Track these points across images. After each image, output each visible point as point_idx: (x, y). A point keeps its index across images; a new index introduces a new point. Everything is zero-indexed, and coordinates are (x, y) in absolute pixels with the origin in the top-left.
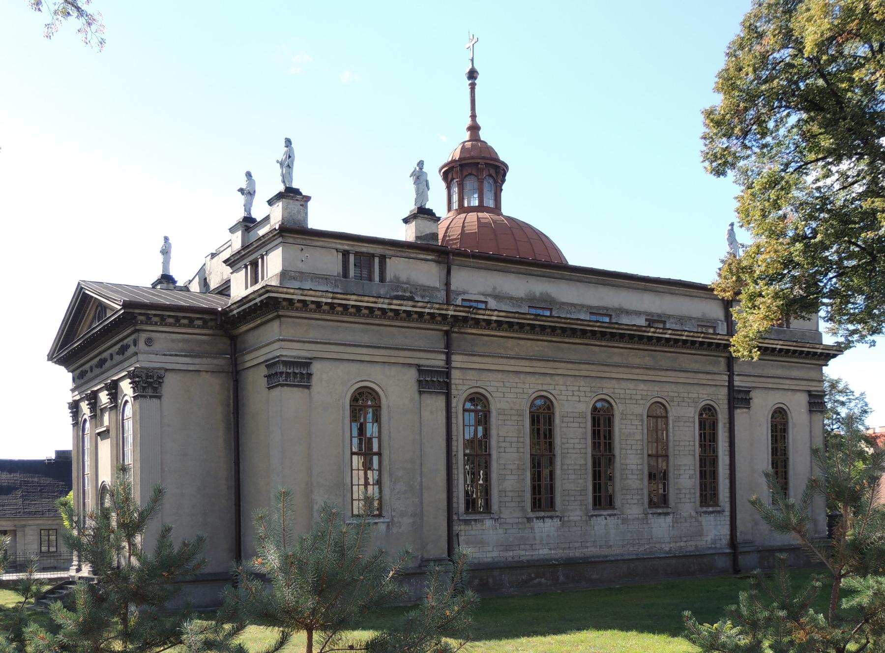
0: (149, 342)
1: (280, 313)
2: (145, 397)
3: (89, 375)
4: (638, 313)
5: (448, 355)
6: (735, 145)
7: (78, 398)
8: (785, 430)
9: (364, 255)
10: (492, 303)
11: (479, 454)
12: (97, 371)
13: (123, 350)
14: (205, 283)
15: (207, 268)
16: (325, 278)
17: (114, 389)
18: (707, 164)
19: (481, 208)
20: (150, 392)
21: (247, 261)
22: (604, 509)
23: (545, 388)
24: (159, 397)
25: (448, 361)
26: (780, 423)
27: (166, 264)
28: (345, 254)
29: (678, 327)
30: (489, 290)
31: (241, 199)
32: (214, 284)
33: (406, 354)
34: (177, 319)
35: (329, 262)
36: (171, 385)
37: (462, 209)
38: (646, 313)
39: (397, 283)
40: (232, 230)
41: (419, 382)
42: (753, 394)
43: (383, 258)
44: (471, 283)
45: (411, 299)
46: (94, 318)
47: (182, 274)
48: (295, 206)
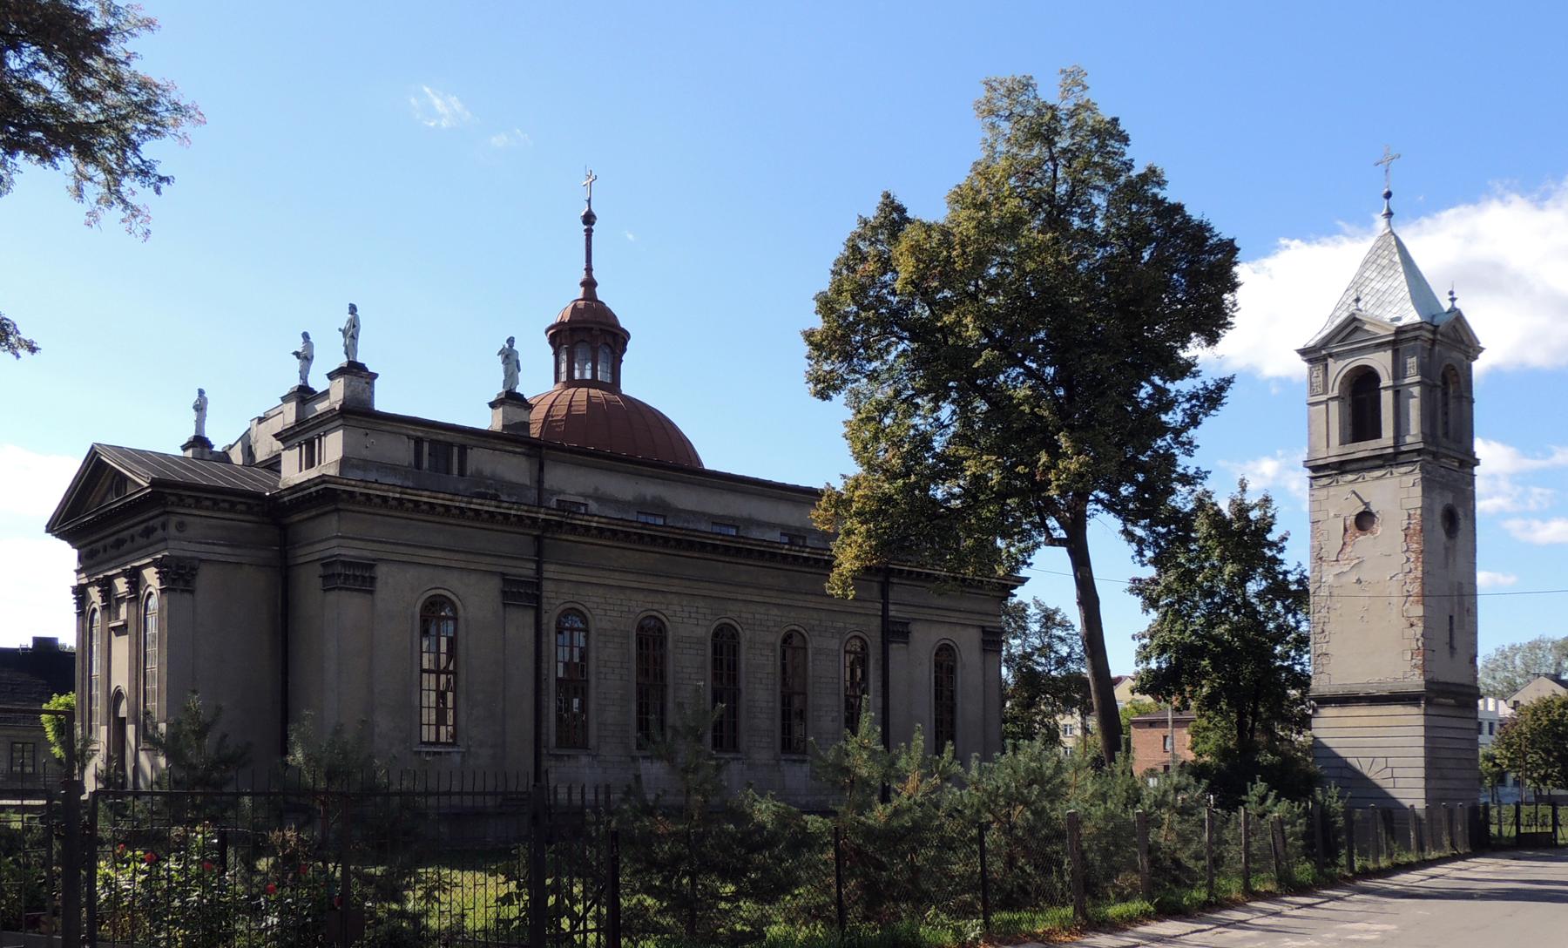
0: (181, 526)
1: (340, 506)
2: (174, 590)
3: (101, 556)
4: (772, 526)
5: (539, 564)
6: (842, 368)
7: (85, 581)
8: (952, 670)
9: (439, 443)
10: (593, 507)
11: (576, 682)
12: (114, 552)
13: (148, 532)
14: (249, 452)
15: (253, 434)
16: (393, 469)
17: (135, 578)
18: (811, 385)
19: (593, 383)
20: (181, 585)
21: (302, 439)
22: (727, 751)
23: (656, 607)
24: (192, 592)
25: (539, 571)
26: (945, 661)
27: (200, 423)
28: (419, 442)
29: (821, 545)
30: (591, 491)
31: (297, 363)
32: (261, 456)
33: (489, 560)
34: (215, 502)
35: (401, 451)
36: (206, 578)
37: (571, 383)
38: (781, 526)
39: (479, 477)
40: (285, 399)
41: (504, 593)
42: (912, 627)
43: (463, 449)
44: (568, 481)
45: (495, 497)
46: (110, 488)
47: (221, 436)
48: (359, 384)
